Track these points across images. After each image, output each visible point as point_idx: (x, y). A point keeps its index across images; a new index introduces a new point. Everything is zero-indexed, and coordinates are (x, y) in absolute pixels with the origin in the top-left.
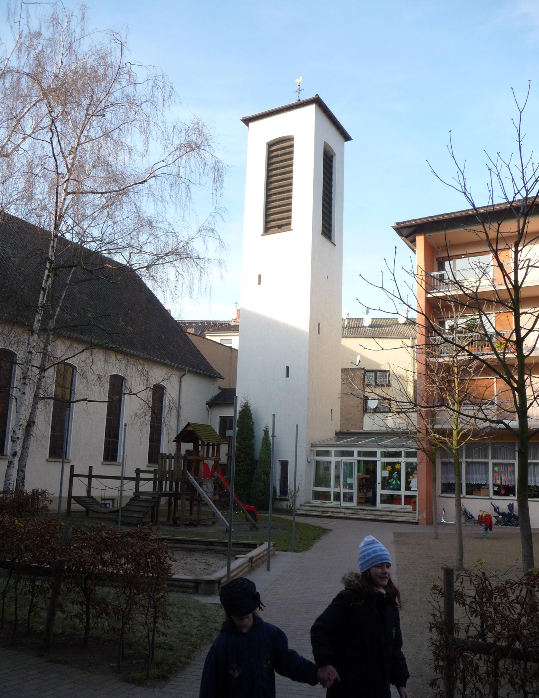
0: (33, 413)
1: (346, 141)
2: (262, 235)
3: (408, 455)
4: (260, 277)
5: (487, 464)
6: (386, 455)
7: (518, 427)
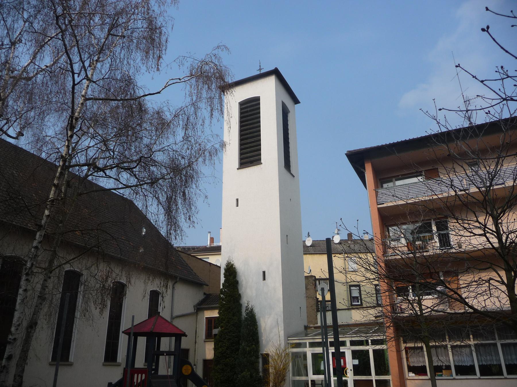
0: (36, 313)
1: (295, 104)
2: (238, 169)
3: (374, 342)
4: (237, 200)
5: (495, 345)
6: (353, 343)
7: (510, 309)
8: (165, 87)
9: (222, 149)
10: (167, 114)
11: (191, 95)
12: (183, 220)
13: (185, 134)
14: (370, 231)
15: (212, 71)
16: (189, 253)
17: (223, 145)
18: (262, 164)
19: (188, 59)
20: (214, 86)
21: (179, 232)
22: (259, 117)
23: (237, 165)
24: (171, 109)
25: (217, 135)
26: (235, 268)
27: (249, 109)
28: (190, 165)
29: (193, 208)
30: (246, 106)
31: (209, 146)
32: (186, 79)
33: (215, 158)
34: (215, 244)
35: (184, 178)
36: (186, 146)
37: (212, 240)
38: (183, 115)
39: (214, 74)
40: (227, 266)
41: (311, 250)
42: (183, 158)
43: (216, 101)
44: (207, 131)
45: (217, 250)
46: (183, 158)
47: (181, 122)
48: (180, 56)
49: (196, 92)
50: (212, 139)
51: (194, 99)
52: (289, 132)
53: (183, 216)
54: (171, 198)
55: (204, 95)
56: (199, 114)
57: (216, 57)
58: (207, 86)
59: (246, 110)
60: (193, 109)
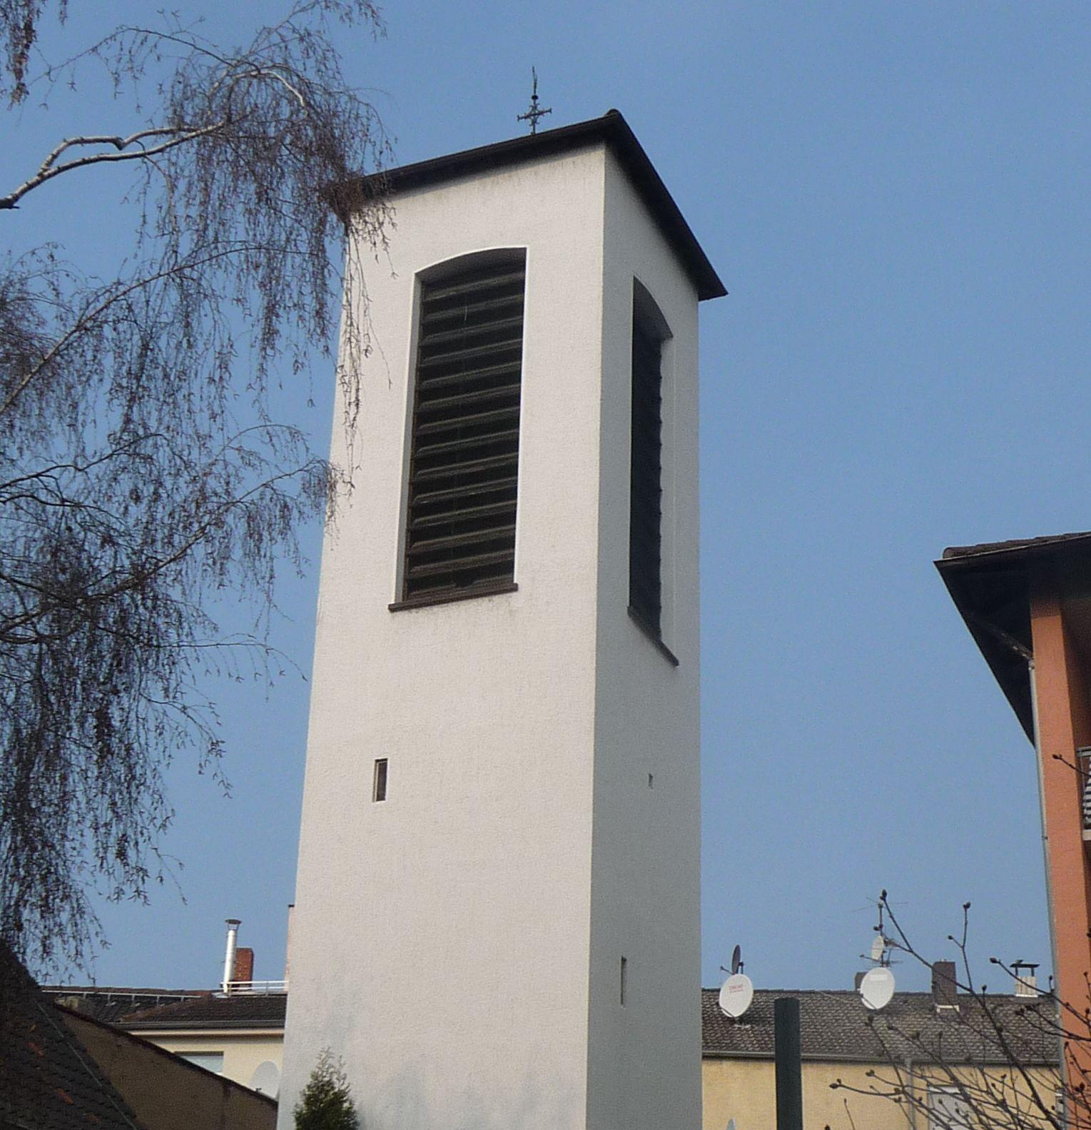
2: (393, 609)
4: (382, 766)
8: (42, 178)
9: (317, 506)
10: (46, 310)
11: (169, 226)
12: (89, 855)
13: (128, 420)
14: (1039, 952)
15: (285, 111)
16: (122, 1022)
17: (322, 484)
18: (514, 588)
19: (166, 47)
20: (287, 191)
21: (64, 917)
22: (517, 354)
23: (389, 589)
24: (67, 288)
25: (294, 434)
26: (349, 1113)
27: (466, 310)
28: (141, 578)
29: (145, 800)
30: (451, 292)
31: (248, 486)
32: (152, 144)
33: (278, 549)
34: (259, 986)
35: (108, 641)
36: (126, 483)
37: (245, 961)
38: (122, 327)
39: (294, 128)
40: (311, 1100)
41: (747, 1038)
42: (108, 540)
43: (293, 266)
44: (241, 412)
45: (264, 1015)
46: (108, 540)
47: (109, 361)
48: (122, 29)
49: (194, 211)
50: (266, 452)
51: (186, 244)
52: (664, 436)
53: (89, 833)
54: (37, 737)
55: (239, 229)
56: (204, 324)
57: (312, 46)
58: (253, 187)
59: (451, 313)
60: (174, 295)
